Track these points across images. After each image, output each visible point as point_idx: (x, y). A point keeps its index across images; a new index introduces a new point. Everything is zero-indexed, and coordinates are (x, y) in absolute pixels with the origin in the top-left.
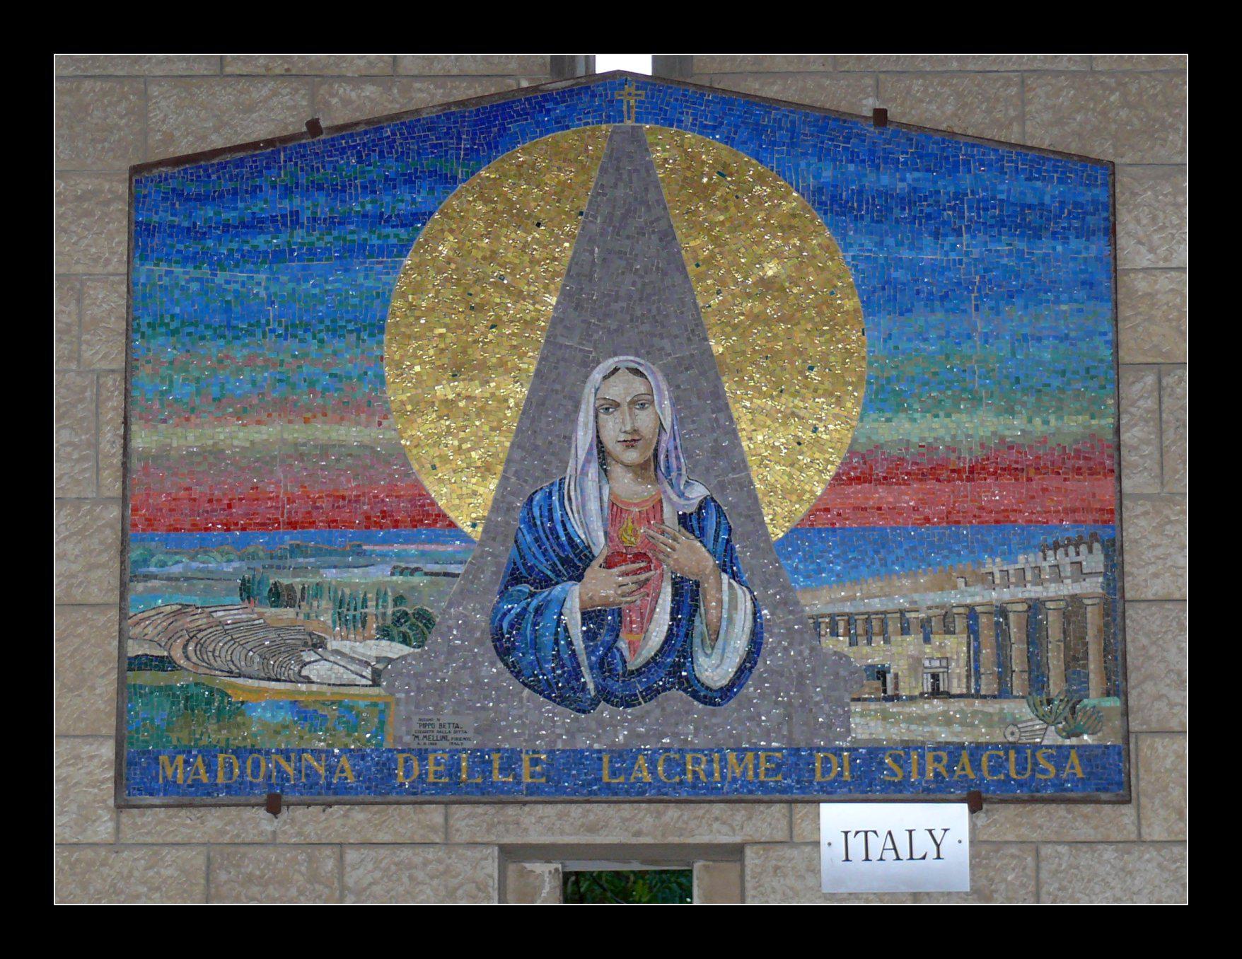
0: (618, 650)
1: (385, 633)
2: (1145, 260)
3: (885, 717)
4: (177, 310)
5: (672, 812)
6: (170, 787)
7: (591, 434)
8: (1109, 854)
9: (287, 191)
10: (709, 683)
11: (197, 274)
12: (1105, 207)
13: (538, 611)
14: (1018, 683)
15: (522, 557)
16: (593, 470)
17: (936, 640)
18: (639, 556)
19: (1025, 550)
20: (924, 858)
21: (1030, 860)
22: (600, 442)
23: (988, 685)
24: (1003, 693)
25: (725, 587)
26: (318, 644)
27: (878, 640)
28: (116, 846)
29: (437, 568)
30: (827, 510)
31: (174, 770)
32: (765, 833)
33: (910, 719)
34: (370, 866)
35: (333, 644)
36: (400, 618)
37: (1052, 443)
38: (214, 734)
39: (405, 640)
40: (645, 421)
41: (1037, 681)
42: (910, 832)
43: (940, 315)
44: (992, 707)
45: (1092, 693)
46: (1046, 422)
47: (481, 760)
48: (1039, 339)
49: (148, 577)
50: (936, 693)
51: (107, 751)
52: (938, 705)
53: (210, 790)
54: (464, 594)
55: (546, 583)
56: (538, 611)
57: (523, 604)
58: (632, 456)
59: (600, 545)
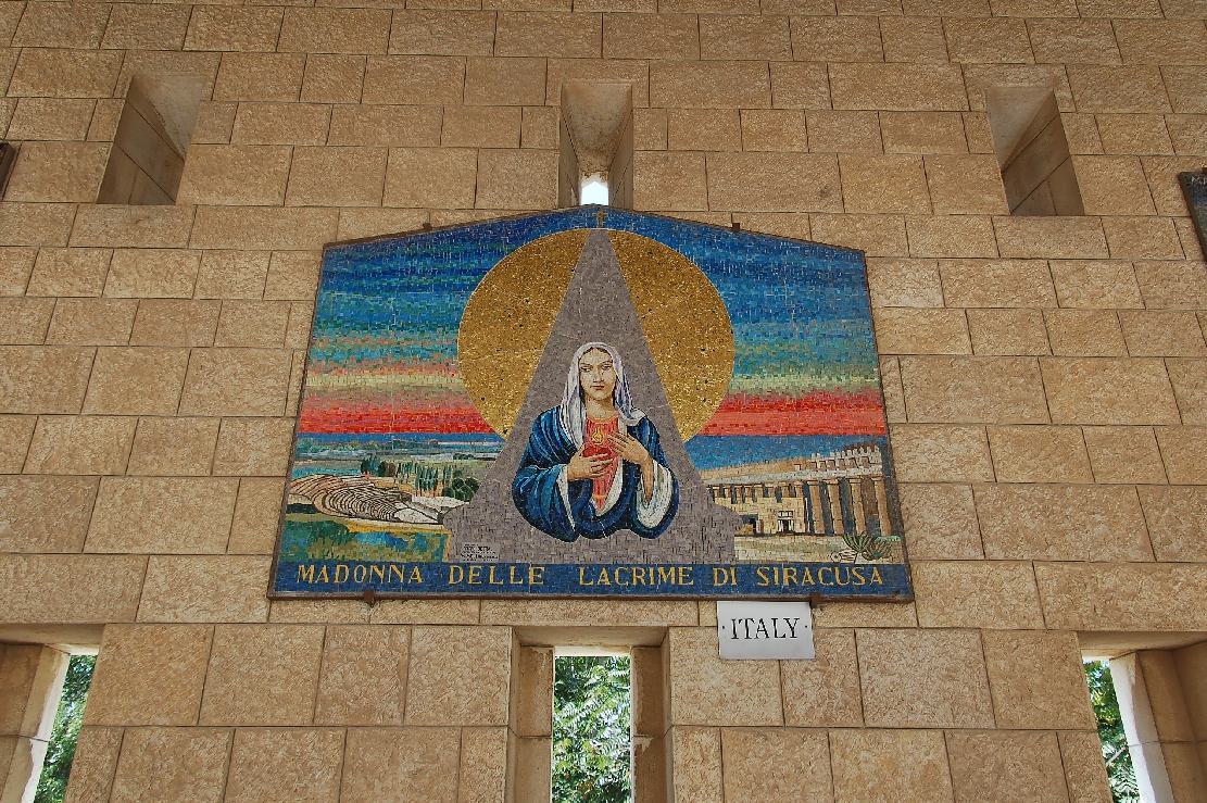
0: (591, 504)
1: (447, 493)
2: (885, 303)
3: (755, 545)
4: (342, 315)
5: (623, 607)
6: (304, 585)
7: (576, 383)
8: (901, 635)
9: (410, 257)
10: (648, 525)
11: (355, 296)
12: (862, 272)
13: (543, 481)
14: (837, 526)
15: (534, 450)
16: (577, 401)
17: (785, 500)
18: (603, 450)
19: (834, 449)
20: (784, 636)
21: (851, 639)
22: (581, 386)
23: (819, 528)
24: (829, 532)
25: (656, 469)
26: (406, 499)
27: (749, 500)
28: (267, 623)
29: (481, 455)
30: (715, 425)
31: (308, 574)
32: (684, 621)
33: (773, 547)
34: (429, 640)
35: (415, 499)
36: (457, 484)
37: (844, 391)
38: (338, 552)
39: (459, 497)
40: (608, 376)
41: (849, 523)
42: (775, 620)
43: (774, 324)
44: (822, 541)
45: (883, 533)
46: (839, 379)
47: (502, 569)
48: (832, 337)
49: (305, 458)
50: (786, 532)
51: (268, 564)
52: (786, 540)
53: (330, 587)
54: (498, 471)
55: (546, 464)
56: (543, 481)
57: (533, 476)
58: (600, 395)
59: (580, 445)
